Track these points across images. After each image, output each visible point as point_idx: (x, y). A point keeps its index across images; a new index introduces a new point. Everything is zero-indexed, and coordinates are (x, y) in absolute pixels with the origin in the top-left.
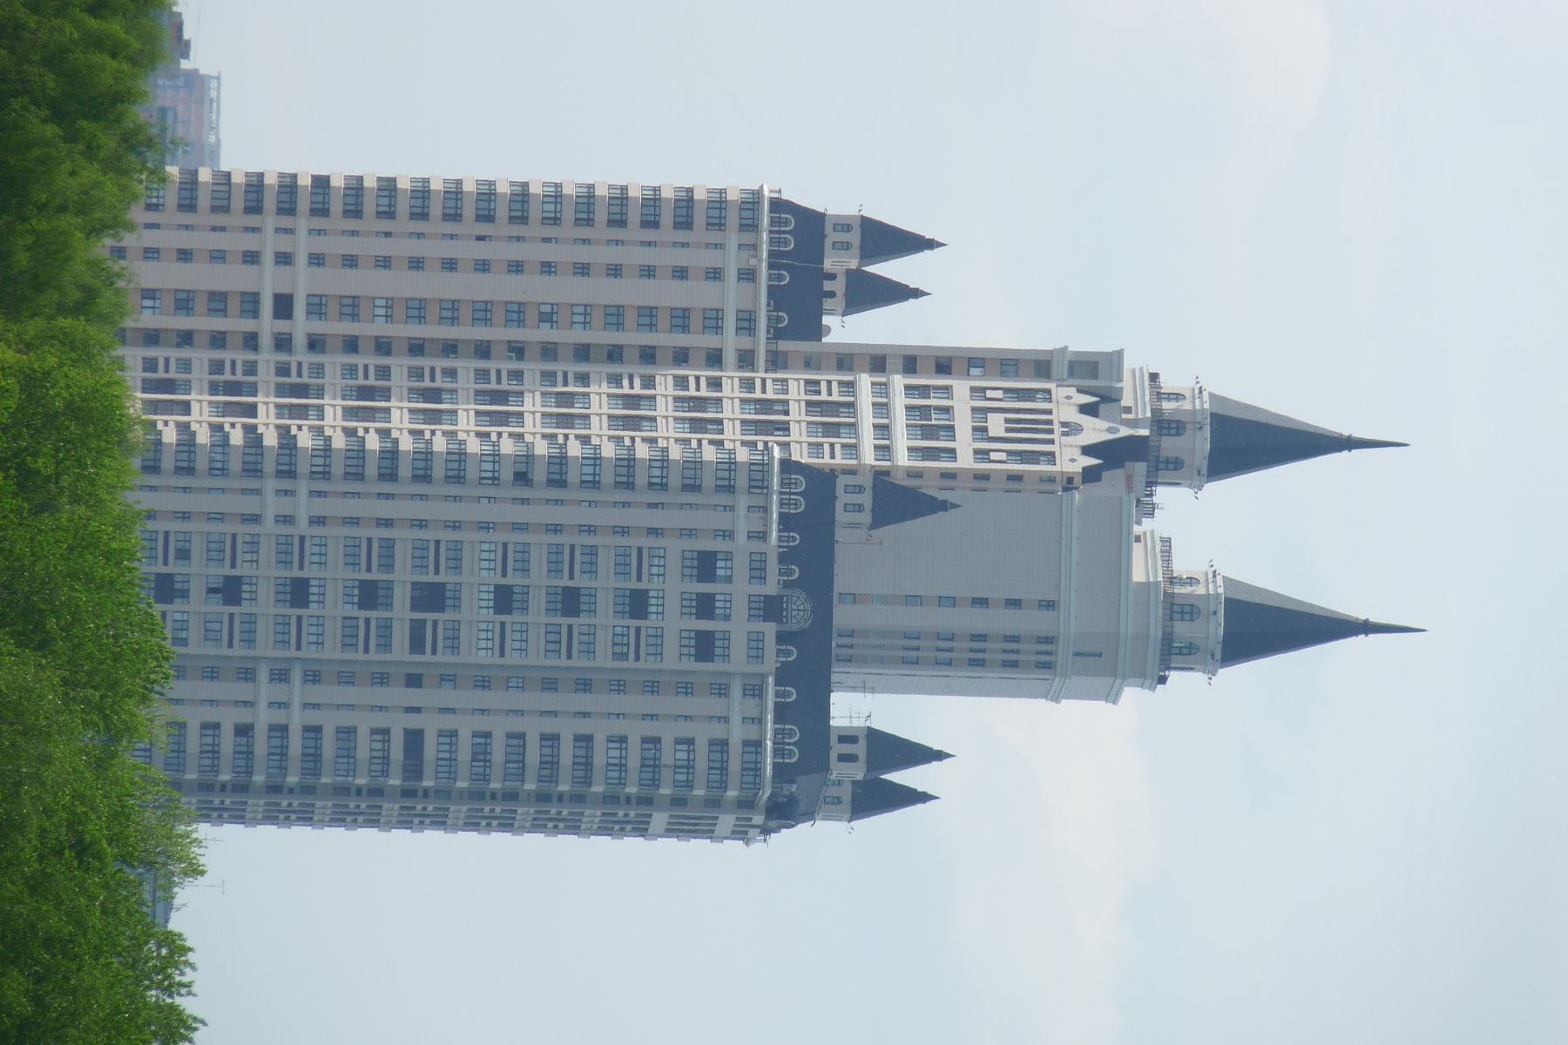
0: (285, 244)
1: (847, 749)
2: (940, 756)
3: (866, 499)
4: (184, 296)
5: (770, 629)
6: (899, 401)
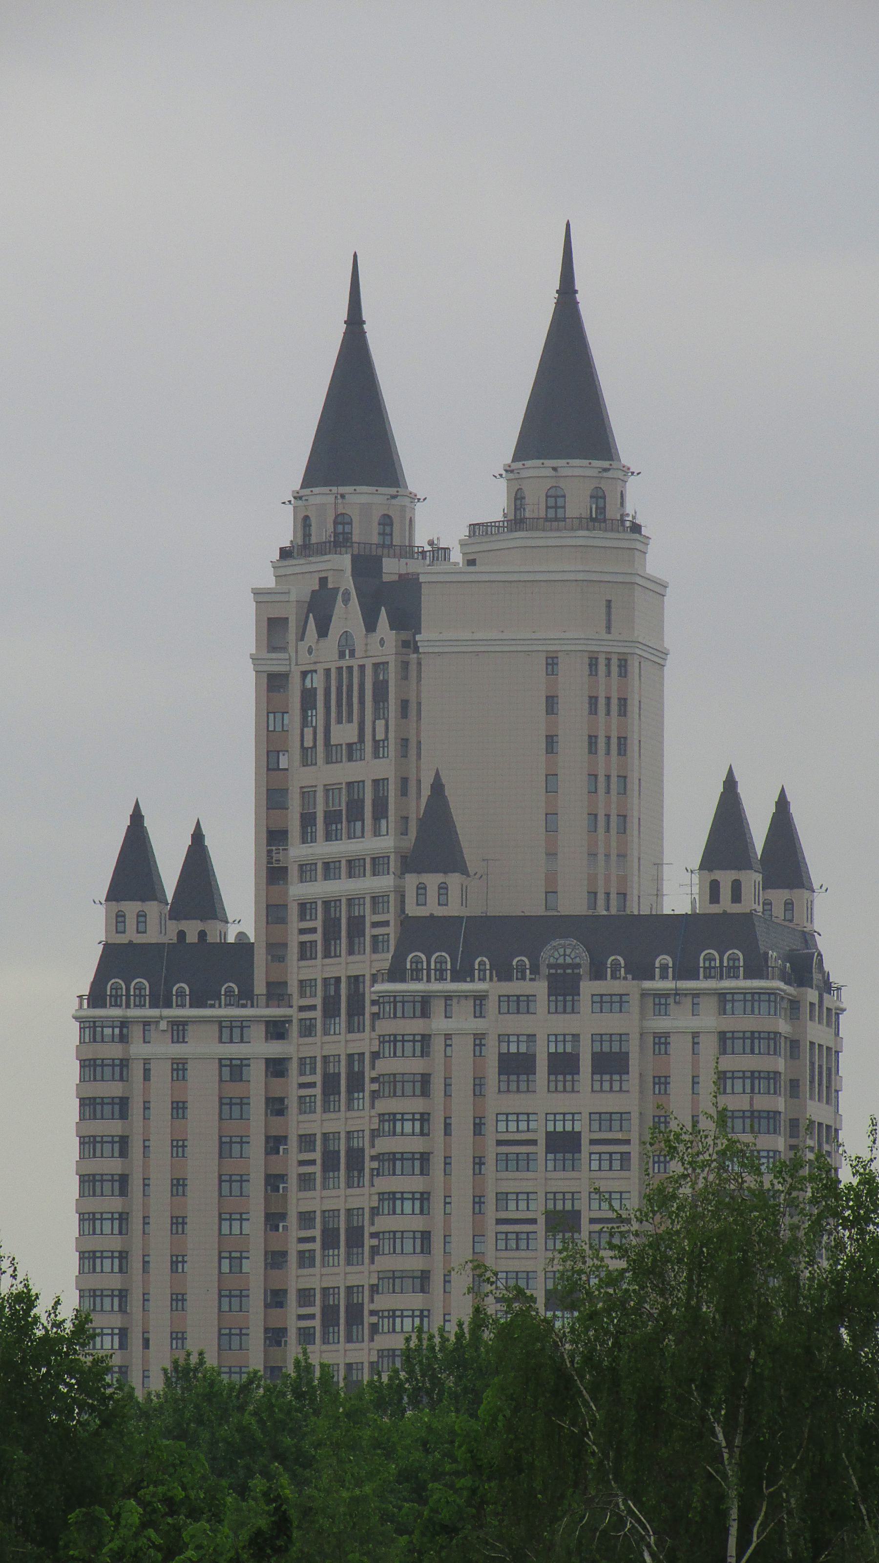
1: (726, 892)
2: (730, 784)
3: (432, 880)
4: (226, 1071)
5: (588, 988)
6: (322, 849)
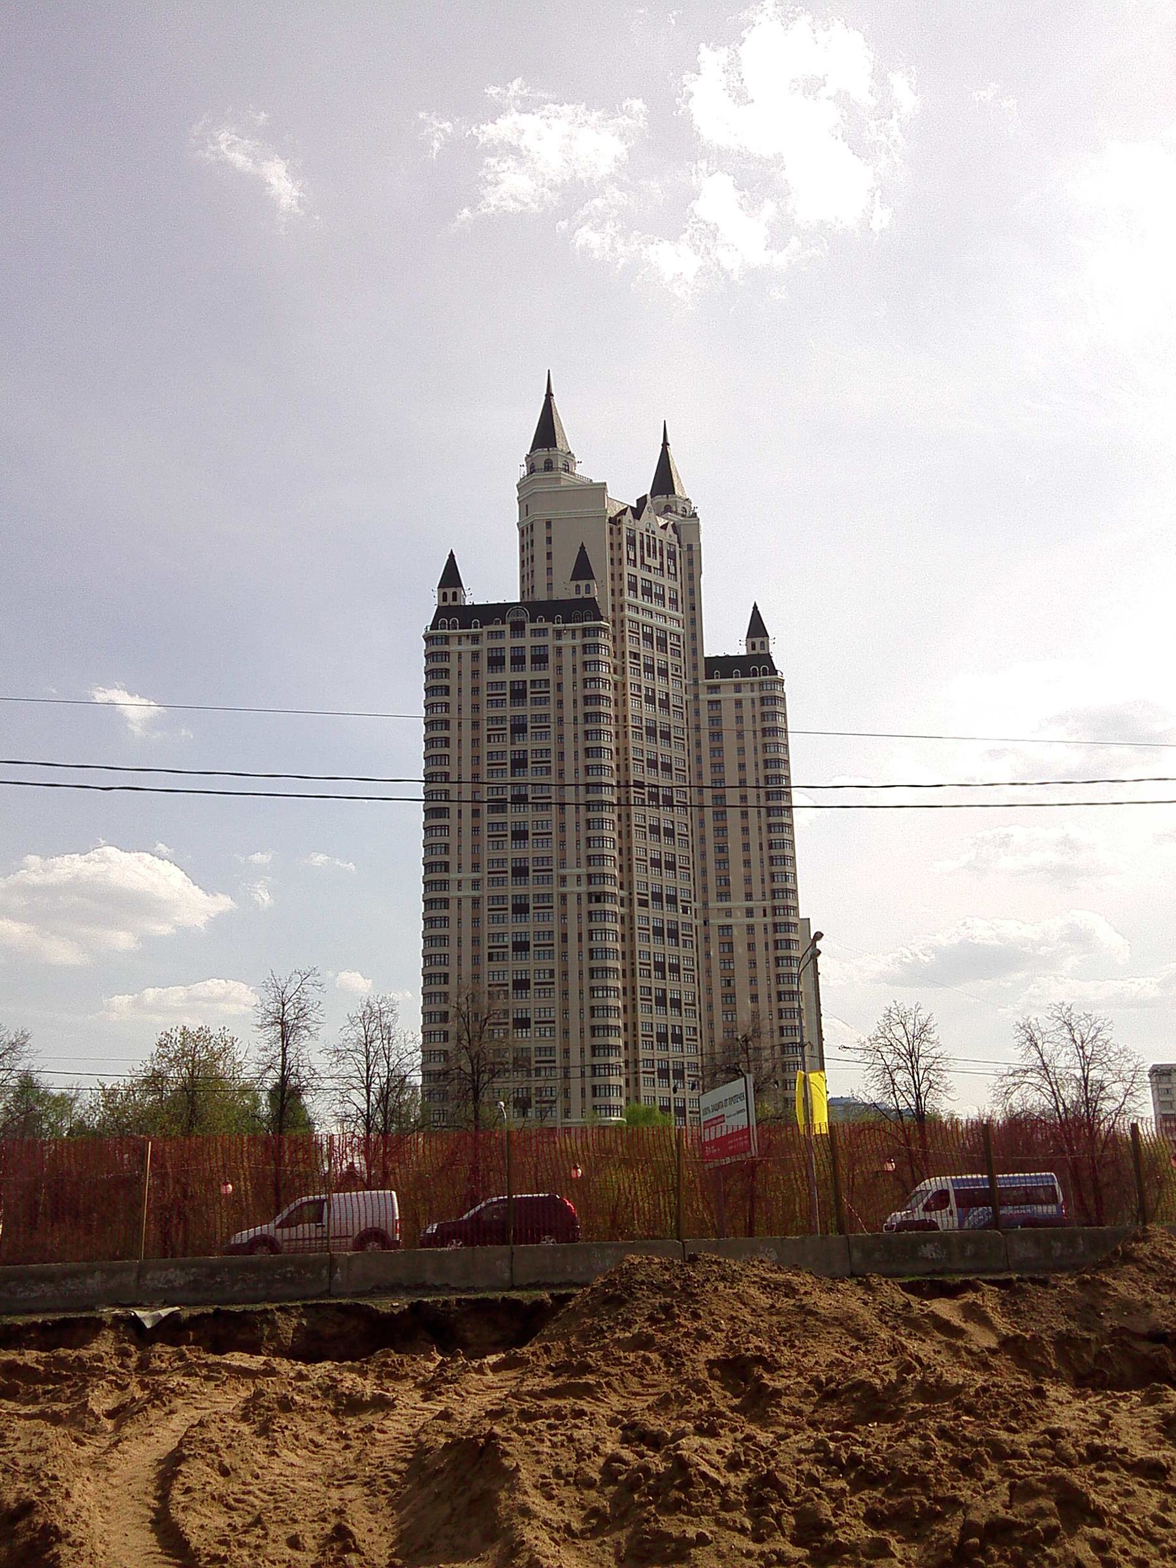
1: (450, 597)
5: (529, 626)
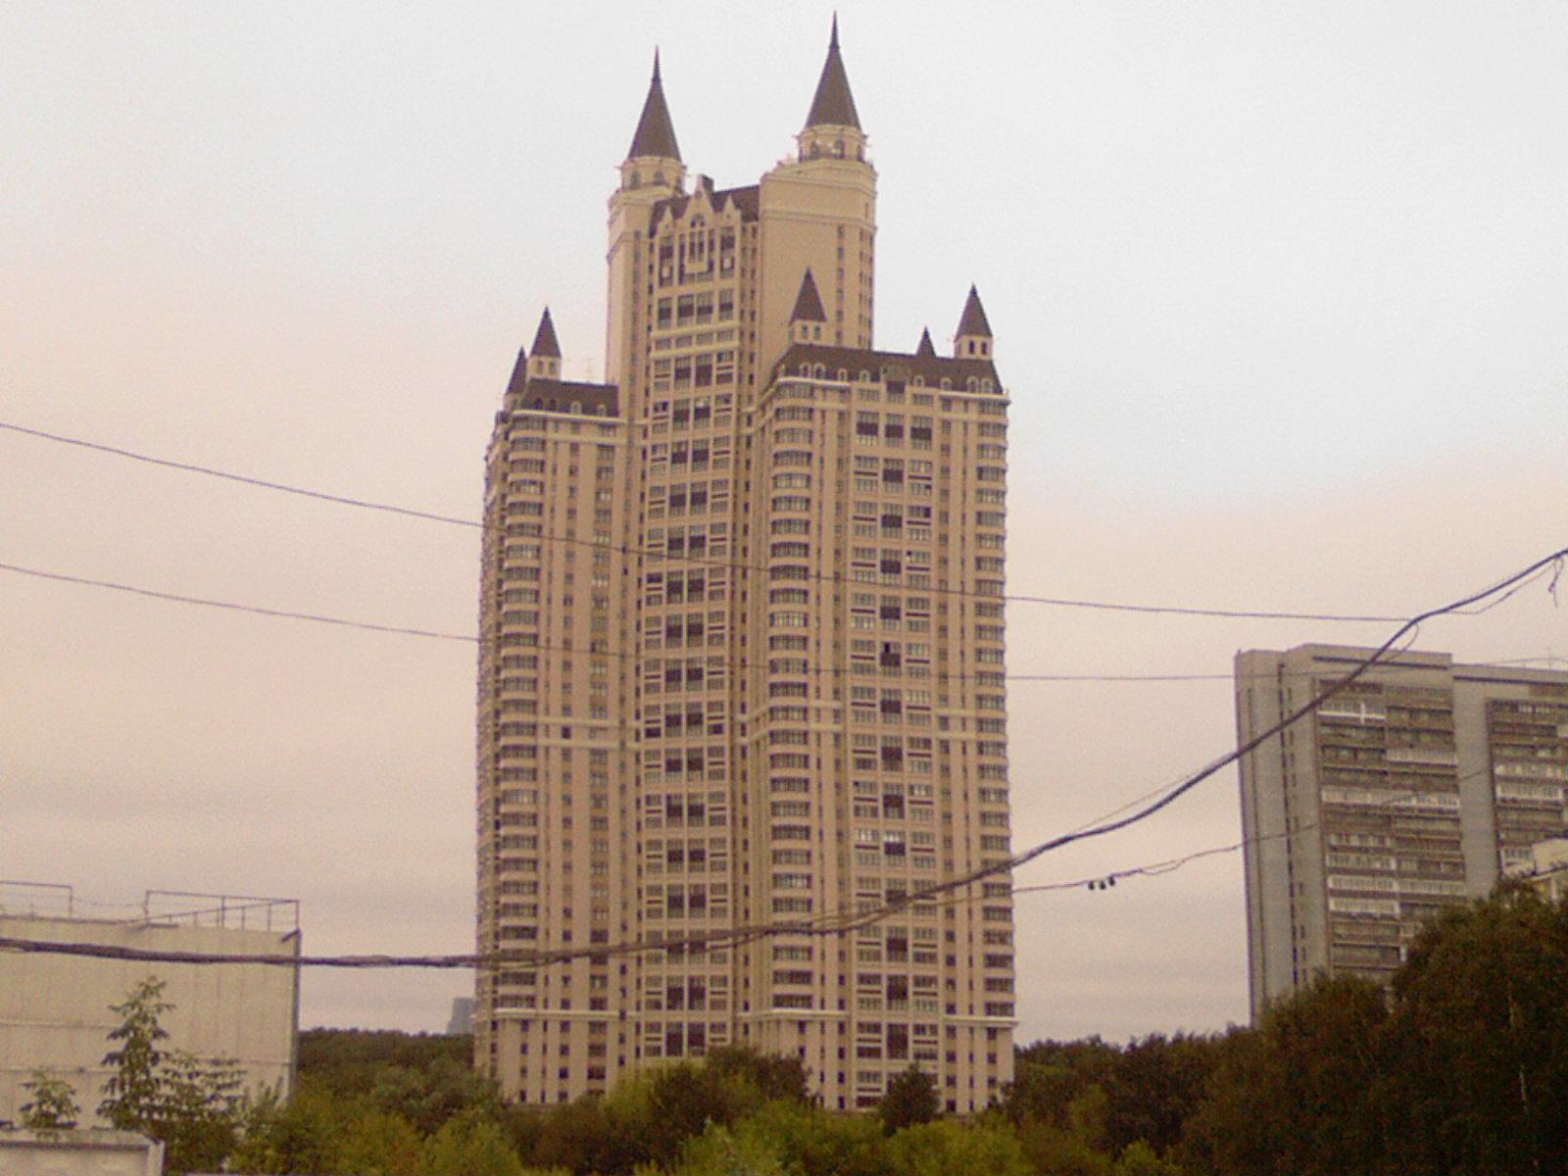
0: (556, 732)
